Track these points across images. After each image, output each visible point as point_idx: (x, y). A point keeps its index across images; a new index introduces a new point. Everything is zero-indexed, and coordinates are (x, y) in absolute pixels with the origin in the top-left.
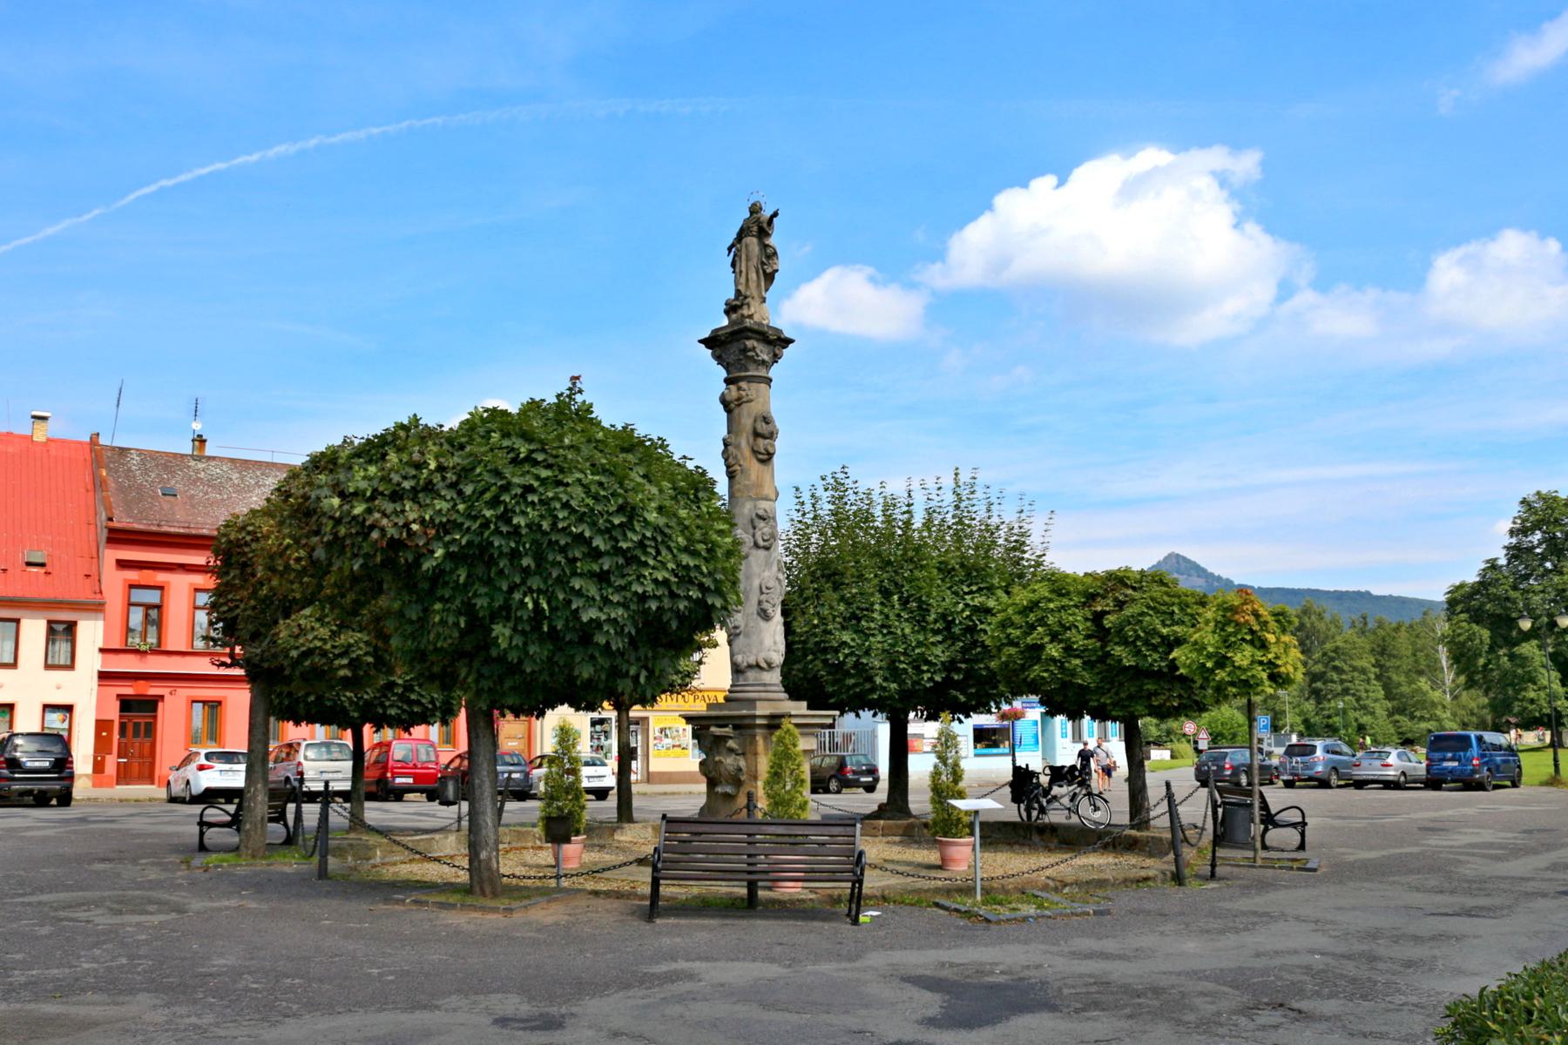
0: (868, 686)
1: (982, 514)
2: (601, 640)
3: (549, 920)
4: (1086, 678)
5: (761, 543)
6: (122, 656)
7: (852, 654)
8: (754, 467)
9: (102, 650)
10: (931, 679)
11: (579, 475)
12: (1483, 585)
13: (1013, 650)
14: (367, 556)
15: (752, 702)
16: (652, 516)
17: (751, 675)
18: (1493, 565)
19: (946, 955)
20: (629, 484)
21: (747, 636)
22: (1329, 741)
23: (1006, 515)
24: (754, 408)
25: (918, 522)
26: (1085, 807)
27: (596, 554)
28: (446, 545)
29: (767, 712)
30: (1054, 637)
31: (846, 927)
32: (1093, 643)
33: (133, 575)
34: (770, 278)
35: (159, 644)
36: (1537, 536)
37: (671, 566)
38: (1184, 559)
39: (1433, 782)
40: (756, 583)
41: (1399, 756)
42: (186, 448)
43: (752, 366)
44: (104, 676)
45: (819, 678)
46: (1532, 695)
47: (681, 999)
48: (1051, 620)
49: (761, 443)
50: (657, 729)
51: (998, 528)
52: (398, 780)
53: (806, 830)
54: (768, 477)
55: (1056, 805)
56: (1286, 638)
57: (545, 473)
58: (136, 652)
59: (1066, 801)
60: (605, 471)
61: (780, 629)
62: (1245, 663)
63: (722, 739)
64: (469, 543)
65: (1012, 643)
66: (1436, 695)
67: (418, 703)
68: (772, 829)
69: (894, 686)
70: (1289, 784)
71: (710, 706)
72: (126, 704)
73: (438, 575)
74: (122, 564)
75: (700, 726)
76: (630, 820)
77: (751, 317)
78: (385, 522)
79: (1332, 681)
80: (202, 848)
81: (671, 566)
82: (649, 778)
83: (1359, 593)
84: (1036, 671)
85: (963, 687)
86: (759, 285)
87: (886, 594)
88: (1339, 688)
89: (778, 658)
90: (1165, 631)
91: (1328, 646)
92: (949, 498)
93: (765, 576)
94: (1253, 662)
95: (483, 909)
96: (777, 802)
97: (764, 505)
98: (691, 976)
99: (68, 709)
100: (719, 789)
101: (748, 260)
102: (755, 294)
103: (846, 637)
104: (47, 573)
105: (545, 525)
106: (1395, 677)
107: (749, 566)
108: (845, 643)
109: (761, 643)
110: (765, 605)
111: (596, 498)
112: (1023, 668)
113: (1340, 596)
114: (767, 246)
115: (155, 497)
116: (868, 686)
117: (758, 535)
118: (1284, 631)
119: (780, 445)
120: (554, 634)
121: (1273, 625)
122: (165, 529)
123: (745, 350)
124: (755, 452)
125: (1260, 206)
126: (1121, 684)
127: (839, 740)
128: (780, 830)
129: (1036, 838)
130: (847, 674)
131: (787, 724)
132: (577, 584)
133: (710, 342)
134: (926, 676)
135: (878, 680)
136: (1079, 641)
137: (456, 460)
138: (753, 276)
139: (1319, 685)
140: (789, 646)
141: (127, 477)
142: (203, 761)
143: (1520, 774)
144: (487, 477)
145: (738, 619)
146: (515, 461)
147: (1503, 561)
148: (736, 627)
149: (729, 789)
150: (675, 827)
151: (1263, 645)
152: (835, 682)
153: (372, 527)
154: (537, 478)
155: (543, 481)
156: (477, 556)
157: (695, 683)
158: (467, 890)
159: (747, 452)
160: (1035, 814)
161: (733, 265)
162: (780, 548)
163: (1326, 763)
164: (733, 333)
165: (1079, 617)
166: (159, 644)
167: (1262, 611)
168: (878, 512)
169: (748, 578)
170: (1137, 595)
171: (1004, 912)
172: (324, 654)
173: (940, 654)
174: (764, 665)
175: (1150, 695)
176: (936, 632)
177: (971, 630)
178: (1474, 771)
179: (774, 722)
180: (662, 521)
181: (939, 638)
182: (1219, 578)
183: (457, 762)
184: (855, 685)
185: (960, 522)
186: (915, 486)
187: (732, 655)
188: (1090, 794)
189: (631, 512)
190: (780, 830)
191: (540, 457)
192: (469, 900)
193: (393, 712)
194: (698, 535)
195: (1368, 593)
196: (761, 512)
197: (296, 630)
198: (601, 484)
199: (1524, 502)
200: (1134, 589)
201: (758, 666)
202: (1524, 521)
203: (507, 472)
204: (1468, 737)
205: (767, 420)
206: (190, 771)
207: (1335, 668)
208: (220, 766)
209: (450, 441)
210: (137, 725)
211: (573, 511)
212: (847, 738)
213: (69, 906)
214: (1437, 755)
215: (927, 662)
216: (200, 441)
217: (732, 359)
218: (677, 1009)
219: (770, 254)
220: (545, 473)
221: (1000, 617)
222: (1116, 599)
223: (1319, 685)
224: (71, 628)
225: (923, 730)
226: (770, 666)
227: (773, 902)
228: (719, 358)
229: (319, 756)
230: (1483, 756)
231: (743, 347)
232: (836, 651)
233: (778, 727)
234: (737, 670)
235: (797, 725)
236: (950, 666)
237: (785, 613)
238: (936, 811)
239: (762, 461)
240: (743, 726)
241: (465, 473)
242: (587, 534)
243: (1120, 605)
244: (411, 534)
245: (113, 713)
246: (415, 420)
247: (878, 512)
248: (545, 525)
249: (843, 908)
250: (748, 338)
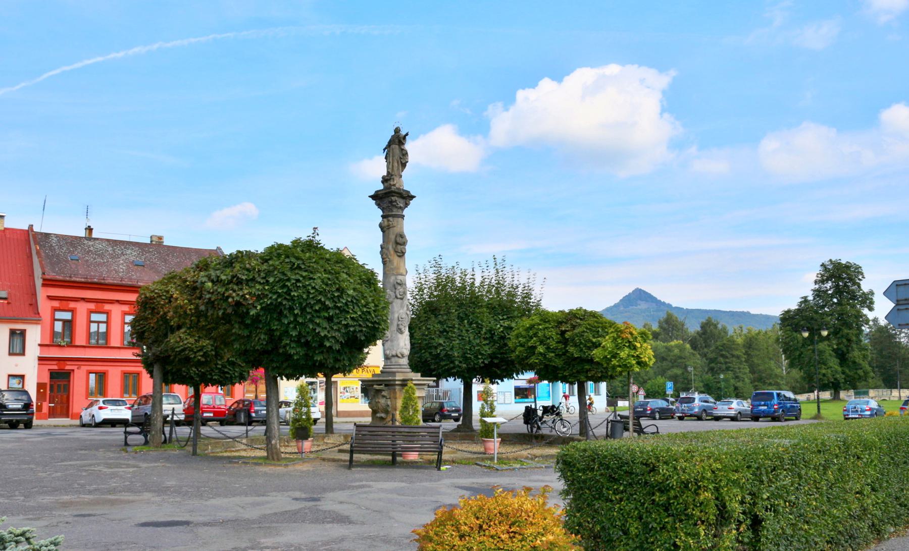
0: (452, 365)
1: (508, 281)
2: (328, 344)
3: (305, 469)
4: (558, 362)
6: (122, 351)
7: (444, 349)
8: (396, 260)
9: (40, 345)
10: (483, 362)
11: (319, 275)
12: (798, 312)
13: (522, 349)
14: (225, 309)
15: (394, 373)
16: (351, 292)
17: (394, 360)
18: (805, 300)
19: (475, 480)
20: (341, 279)
21: (392, 341)
22: (702, 396)
23: (521, 279)
24: (396, 230)
25: (477, 284)
26: (558, 424)
27: (327, 308)
28: (261, 304)
29: (401, 378)
30: (542, 342)
31: (435, 472)
32: (561, 346)
33: (56, 304)
34: (404, 165)
35: (71, 342)
36: (829, 285)
37: (359, 313)
39: (755, 418)
40: (396, 316)
41: (738, 404)
42: (82, 233)
43: (395, 210)
44: (41, 359)
45: (428, 362)
46: (824, 371)
47: (365, 493)
48: (540, 334)
49: (399, 247)
50: (342, 387)
51: (517, 287)
52: (205, 415)
53: (419, 430)
54: (402, 264)
55: (545, 425)
56: (645, 345)
57: (304, 274)
58: (59, 346)
59: (550, 423)
60: (330, 273)
61: (408, 338)
62: (625, 356)
63: (379, 391)
64: (271, 303)
65: (522, 345)
66: (778, 371)
67: (228, 373)
68: (402, 430)
69: (464, 365)
70: (681, 418)
71: (374, 375)
72: (53, 375)
73: (256, 319)
74: (50, 298)
75: (368, 389)
76: (332, 432)
77: (394, 185)
78: (234, 294)
79: (721, 363)
80: (126, 444)
81: (359, 313)
82: (339, 414)
83: (743, 312)
84: (533, 360)
85: (497, 368)
86: (398, 169)
87: (461, 319)
88: (724, 367)
89: (407, 351)
90: (594, 340)
91: (719, 343)
92: (493, 271)
93: (401, 312)
94: (628, 355)
95: (274, 465)
96: (406, 420)
97: (400, 277)
98: (369, 486)
99: (22, 377)
100: (378, 415)
101: (393, 156)
103: (441, 341)
104: (8, 303)
105: (305, 296)
106: (756, 361)
107: (393, 307)
108: (440, 344)
110: (401, 327)
111: (327, 285)
112: (527, 358)
113: (732, 314)
114: (403, 150)
115: (67, 261)
116: (452, 365)
117: (397, 292)
118: (645, 342)
119: (408, 248)
120: (307, 344)
121: (639, 338)
122: (74, 279)
123: (391, 202)
125: (673, 103)
126: (573, 366)
127: (441, 394)
128: (407, 430)
129: (534, 441)
130: (442, 360)
131: (410, 384)
132: (317, 321)
134: (480, 361)
135: (457, 363)
136: (553, 344)
137: (265, 267)
139: (713, 365)
140: (412, 344)
141: (50, 249)
142: (102, 405)
143: (800, 414)
144: (279, 275)
145: (388, 333)
146: (292, 269)
147: (811, 298)
149: (383, 415)
150: (360, 429)
151: (635, 348)
152: (435, 364)
153: (228, 297)
154: (301, 276)
155: (304, 277)
156: (274, 310)
157: (365, 364)
158: (267, 458)
159: (392, 252)
160: (535, 430)
161: (386, 158)
162: (409, 296)
163: (700, 407)
164: (386, 193)
165: (553, 333)
166: (71, 342)
167: (634, 332)
168: (458, 279)
169: (393, 313)
170: (582, 322)
171: (505, 467)
172: (191, 350)
173: (487, 350)
175: (587, 371)
176: (485, 339)
177: (503, 338)
178: (775, 412)
179: (404, 383)
180: (355, 294)
181: (487, 342)
183: (236, 405)
184: (446, 365)
185: (499, 283)
186: (476, 266)
187: (384, 351)
188: (561, 419)
189: (341, 290)
190: (407, 430)
191: (303, 267)
192: (268, 462)
193: (216, 377)
194: (370, 299)
195: (748, 313)
197: (178, 339)
198: (329, 279)
199: (823, 265)
200: (581, 319)
201: (397, 356)
202: (822, 276)
203: (289, 274)
204: (772, 394)
205: (402, 236)
206: (94, 410)
207: (722, 356)
208: (110, 407)
209: (261, 258)
210: (59, 386)
211: (317, 290)
212: (446, 393)
213: (90, 465)
214: (758, 403)
215: (482, 354)
216: (90, 229)
217: (385, 206)
218: (365, 496)
219: (404, 154)
220: (304, 274)
221: (515, 332)
222: (572, 324)
223: (713, 365)
224: (23, 333)
225: (477, 387)
226: (403, 356)
227: (403, 462)
228: (379, 205)
229: (175, 402)
230: (780, 404)
231: (391, 199)
232: (436, 348)
233: (406, 385)
234: (387, 358)
235: (415, 385)
236: (492, 356)
237: (410, 328)
238: (482, 425)
240: (389, 385)
241: (269, 273)
242: (323, 300)
243: (574, 327)
244: (246, 299)
245: (46, 379)
247: (458, 279)
248: (305, 296)
249: (435, 465)
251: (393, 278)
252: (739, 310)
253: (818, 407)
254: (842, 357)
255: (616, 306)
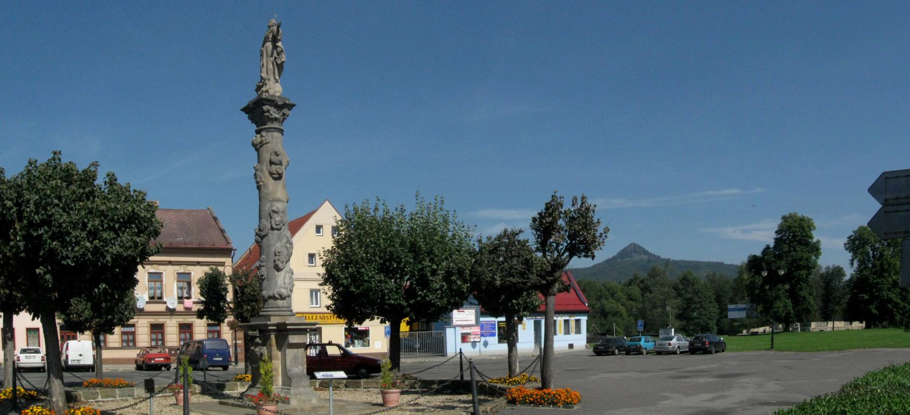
5: (275, 226)
8: (270, 182)
18: (768, 247)
21: (268, 280)
38: (639, 247)
49: (274, 168)
77: (267, 91)
102: (272, 79)
109: (276, 284)
124: (271, 174)
133: (246, 110)
138: (271, 66)
148: (262, 276)
159: (267, 174)
174: (277, 296)
182: (654, 256)
195: (722, 263)
196: (274, 209)
239: (275, 179)
246: (506, 231)
250: (264, 105)
251: (268, 205)
252: (716, 261)
253: (772, 340)
254: (793, 295)
255: (614, 258)
